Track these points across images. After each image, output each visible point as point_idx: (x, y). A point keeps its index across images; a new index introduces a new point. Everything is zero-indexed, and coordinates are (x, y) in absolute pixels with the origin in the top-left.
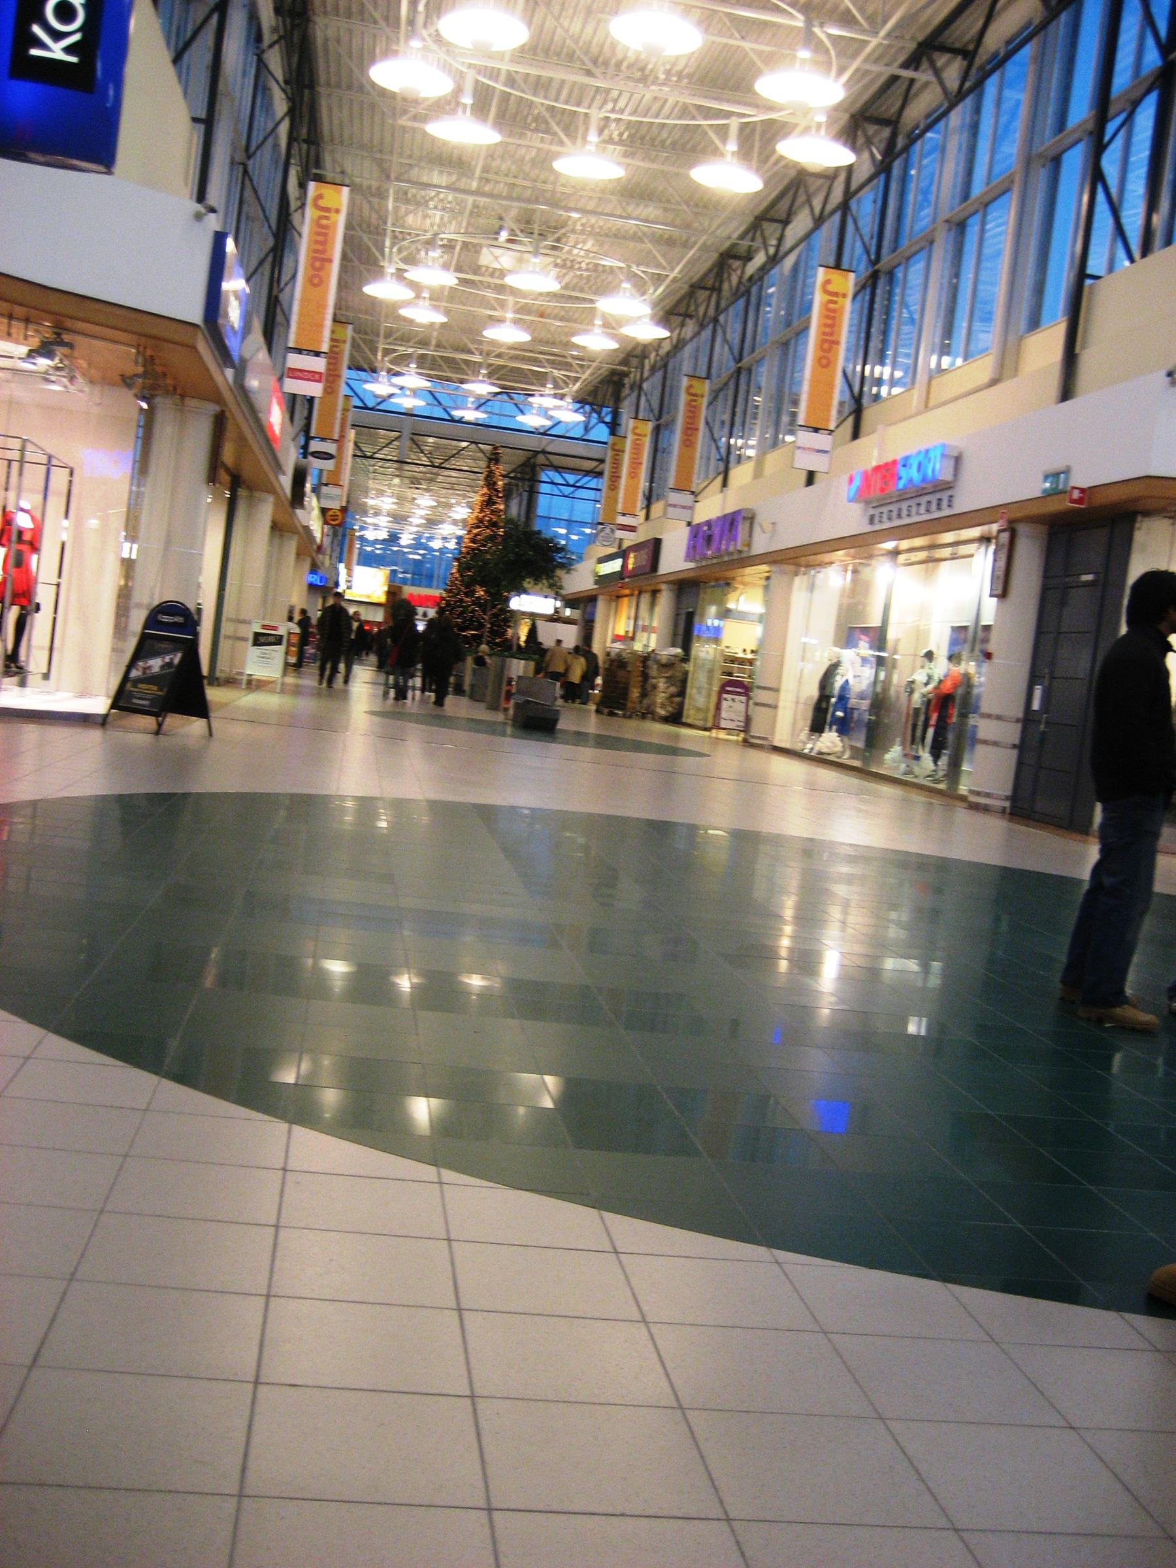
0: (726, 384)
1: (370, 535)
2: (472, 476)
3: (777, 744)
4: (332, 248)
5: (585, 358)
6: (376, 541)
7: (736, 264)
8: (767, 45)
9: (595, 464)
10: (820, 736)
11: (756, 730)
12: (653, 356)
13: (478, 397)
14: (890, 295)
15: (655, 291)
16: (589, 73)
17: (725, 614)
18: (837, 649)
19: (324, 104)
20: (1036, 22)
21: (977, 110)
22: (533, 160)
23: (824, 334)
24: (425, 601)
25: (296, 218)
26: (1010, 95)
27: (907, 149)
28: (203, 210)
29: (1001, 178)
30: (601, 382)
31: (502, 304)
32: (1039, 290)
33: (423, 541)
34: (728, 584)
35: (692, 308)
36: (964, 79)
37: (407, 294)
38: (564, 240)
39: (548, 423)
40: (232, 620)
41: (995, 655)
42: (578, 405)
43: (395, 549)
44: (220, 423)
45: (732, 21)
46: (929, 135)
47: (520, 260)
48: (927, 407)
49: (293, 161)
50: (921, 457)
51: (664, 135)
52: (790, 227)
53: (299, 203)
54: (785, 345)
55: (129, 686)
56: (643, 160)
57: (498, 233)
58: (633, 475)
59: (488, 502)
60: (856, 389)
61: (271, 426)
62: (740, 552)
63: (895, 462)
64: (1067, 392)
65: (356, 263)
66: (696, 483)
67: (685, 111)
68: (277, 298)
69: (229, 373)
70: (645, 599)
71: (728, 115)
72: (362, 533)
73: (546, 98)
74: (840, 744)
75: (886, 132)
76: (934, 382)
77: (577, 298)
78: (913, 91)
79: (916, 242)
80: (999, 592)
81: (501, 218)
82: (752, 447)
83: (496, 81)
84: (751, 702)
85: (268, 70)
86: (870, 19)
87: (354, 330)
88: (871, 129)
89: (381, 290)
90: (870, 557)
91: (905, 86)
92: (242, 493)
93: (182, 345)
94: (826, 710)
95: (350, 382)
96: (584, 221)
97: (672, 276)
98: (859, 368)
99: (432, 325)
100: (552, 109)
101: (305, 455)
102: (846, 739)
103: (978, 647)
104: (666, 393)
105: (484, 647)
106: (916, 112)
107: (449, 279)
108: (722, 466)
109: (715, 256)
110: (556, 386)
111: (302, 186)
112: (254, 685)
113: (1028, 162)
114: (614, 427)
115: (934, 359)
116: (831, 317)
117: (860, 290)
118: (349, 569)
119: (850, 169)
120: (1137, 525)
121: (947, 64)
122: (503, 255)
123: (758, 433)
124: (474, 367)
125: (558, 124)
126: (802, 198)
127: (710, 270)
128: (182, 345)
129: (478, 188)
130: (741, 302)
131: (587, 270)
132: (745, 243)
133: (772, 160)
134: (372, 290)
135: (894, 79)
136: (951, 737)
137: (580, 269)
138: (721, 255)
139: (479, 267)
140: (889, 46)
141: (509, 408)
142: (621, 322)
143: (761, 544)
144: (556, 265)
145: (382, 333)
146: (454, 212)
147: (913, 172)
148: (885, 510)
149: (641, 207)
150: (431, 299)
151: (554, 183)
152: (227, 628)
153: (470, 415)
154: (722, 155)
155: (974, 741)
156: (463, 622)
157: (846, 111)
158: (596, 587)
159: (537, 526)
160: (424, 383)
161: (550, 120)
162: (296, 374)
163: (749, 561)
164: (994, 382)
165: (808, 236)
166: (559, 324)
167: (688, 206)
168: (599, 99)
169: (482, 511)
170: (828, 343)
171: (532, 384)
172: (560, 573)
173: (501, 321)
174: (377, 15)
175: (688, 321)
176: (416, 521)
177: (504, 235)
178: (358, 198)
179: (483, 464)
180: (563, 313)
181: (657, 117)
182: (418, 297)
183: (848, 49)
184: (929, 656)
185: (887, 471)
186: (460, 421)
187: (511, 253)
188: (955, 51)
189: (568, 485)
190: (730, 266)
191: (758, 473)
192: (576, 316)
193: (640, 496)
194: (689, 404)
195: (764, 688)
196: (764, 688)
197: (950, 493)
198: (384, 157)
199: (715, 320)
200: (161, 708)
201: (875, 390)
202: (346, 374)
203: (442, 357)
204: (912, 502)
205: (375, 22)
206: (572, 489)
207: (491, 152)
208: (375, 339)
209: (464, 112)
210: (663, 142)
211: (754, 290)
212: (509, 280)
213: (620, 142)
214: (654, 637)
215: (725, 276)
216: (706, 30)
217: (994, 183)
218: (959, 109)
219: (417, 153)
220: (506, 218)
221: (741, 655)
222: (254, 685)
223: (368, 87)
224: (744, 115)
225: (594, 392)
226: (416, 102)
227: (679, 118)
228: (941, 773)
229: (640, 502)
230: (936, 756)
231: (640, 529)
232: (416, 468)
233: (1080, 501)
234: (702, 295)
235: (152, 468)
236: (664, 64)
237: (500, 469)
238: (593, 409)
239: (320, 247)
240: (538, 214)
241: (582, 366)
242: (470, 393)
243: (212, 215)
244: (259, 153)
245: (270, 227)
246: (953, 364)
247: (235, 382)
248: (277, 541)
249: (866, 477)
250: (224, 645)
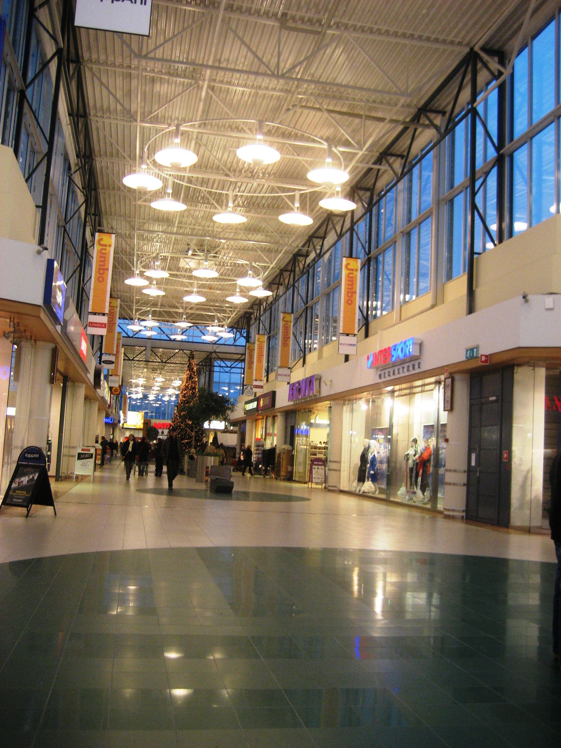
0: (301, 315)
1: (134, 396)
2: (181, 365)
3: (341, 488)
4: (108, 264)
5: (233, 306)
6: (137, 399)
7: (301, 258)
8: (310, 157)
9: (240, 356)
10: (364, 484)
11: (331, 482)
12: (264, 304)
13: (182, 329)
14: (377, 269)
15: (264, 273)
16: (227, 175)
17: (310, 425)
18: (367, 440)
19: (101, 197)
20: (435, 140)
21: (411, 181)
22: (202, 217)
23: (348, 289)
24: (163, 426)
25: (90, 250)
26: (425, 174)
27: (378, 201)
28: (41, 249)
29: (425, 211)
30: (241, 318)
31: (191, 284)
32: (450, 260)
33: (160, 397)
34: (311, 411)
35: (282, 280)
36: (404, 167)
37: (145, 283)
38: (219, 253)
39: (216, 339)
40: (66, 447)
41: (450, 440)
42: (230, 329)
43: (147, 402)
44: (55, 353)
45: (293, 148)
46: (388, 194)
47: (199, 264)
48: (401, 320)
49: (88, 224)
50: (402, 345)
51: (264, 201)
52: (326, 240)
53: (92, 243)
54: (328, 295)
55: (11, 493)
56: (254, 213)
57: (187, 251)
58: (260, 361)
59: (190, 378)
60: (365, 313)
61: (82, 351)
62: (315, 396)
63: (389, 348)
64: (471, 309)
65: (120, 269)
66: (291, 363)
67: (273, 190)
68: (83, 288)
69: (59, 328)
70: (270, 420)
71: (294, 190)
72: (131, 395)
73: (207, 187)
74: (374, 487)
75: (368, 194)
76: (403, 308)
77: (227, 279)
78: (379, 174)
79: (387, 243)
80: (449, 408)
81: (188, 245)
82: (316, 343)
83: (183, 181)
84: (327, 468)
85: (75, 183)
86: (358, 143)
87: (121, 301)
88: (361, 193)
89: (133, 282)
90: (381, 394)
91: (376, 172)
92: (69, 384)
93: (33, 316)
94: (365, 471)
95: (121, 325)
96: (228, 243)
97: (271, 266)
98: (365, 303)
99: (158, 296)
100: (210, 193)
101: (100, 363)
102: (376, 484)
103: (441, 435)
104: (272, 319)
105: (193, 450)
106: (381, 184)
107: (165, 274)
108: (302, 355)
109: (291, 256)
110: (219, 321)
111: (93, 235)
112: (79, 479)
113: (438, 203)
114: (248, 338)
115: (402, 296)
116: (351, 281)
117: (363, 267)
118: (125, 413)
119: (353, 212)
120: (515, 371)
121: (394, 161)
122: (190, 262)
123: (318, 337)
124: (180, 315)
125: (214, 199)
126: (330, 226)
127: (289, 263)
128: (33, 316)
129: (177, 231)
130: (305, 276)
131: (231, 266)
132: (305, 249)
133: (317, 209)
134: (129, 282)
135: (370, 170)
136: (430, 480)
137: (227, 266)
138: (294, 255)
139: (179, 268)
140: (367, 155)
141: (197, 332)
143: (325, 392)
144: (216, 265)
145: (135, 301)
146: (166, 243)
147: (382, 211)
148: (387, 371)
149: (255, 235)
150: (157, 284)
151: (213, 227)
152: (64, 451)
153: (179, 338)
154: (292, 209)
155: (444, 483)
156: (182, 436)
157: (349, 185)
159: (214, 390)
160: (156, 324)
161: (210, 198)
162: (93, 325)
163: (319, 399)
164: (433, 306)
165: (335, 244)
166: (218, 292)
167: (277, 232)
168: (232, 187)
169: (187, 382)
170: (351, 293)
171: (208, 321)
172: (229, 412)
173: (191, 293)
174: (125, 155)
175: (280, 286)
176: (156, 388)
177: (190, 252)
178: (120, 240)
179: (187, 359)
180: (220, 287)
181: (260, 193)
182: (151, 283)
183: (349, 157)
184: (415, 441)
185: (386, 353)
186: (174, 340)
187: (194, 260)
188: (398, 156)
189: (227, 367)
190: (298, 260)
191: (320, 357)
192: (227, 287)
193: (264, 371)
195: (333, 462)
196: (333, 462)
197: (418, 361)
198: (131, 219)
199: (294, 286)
200: (27, 504)
201: (374, 312)
202: (118, 321)
203: (164, 311)
204: (400, 367)
205: (124, 158)
206: (229, 369)
207: (182, 214)
208: (132, 304)
209: (169, 197)
210: (263, 205)
211: (311, 271)
212: (195, 273)
213: (243, 206)
214: (275, 438)
215: (297, 264)
216: (281, 153)
217: (422, 214)
218: (402, 181)
219: (147, 217)
220: (191, 244)
221: (319, 445)
222: (79, 479)
223: (122, 188)
224: (301, 190)
225: (238, 322)
226: (145, 193)
227: (271, 193)
228: (426, 500)
229: (264, 374)
230: (423, 491)
231: (264, 387)
232: (154, 364)
233: (486, 361)
234: (286, 274)
235: (21, 378)
236: (262, 169)
237: (195, 362)
238: (237, 331)
239: (103, 263)
240: (206, 242)
241: (231, 311)
242: (179, 327)
243: (45, 251)
244: (71, 221)
245: (78, 256)
246: (411, 298)
247: (62, 332)
248: (88, 404)
249: (376, 356)
250: (64, 460)
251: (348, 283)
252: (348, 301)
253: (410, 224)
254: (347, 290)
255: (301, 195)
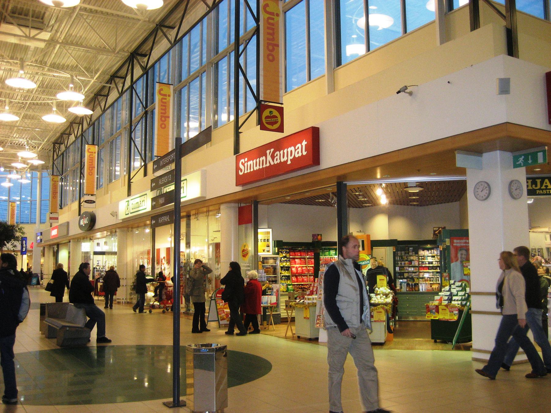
23: (89, 165)
35: (62, 140)
119: (92, 115)
135: (104, 87)
142: (69, 104)
158: (239, 189)
194: (161, 101)
211: (96, 123)
251: (89, 161)
252: (268, 55)
253: (181, 83)
254: (160, 115)
255: (57, 102)
